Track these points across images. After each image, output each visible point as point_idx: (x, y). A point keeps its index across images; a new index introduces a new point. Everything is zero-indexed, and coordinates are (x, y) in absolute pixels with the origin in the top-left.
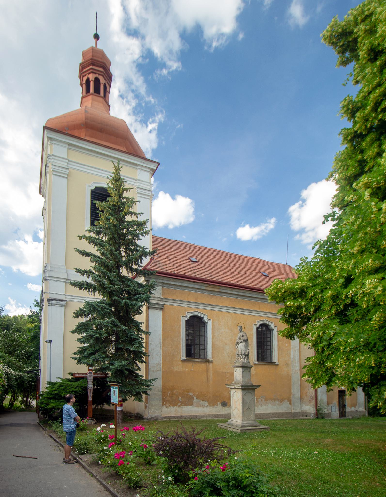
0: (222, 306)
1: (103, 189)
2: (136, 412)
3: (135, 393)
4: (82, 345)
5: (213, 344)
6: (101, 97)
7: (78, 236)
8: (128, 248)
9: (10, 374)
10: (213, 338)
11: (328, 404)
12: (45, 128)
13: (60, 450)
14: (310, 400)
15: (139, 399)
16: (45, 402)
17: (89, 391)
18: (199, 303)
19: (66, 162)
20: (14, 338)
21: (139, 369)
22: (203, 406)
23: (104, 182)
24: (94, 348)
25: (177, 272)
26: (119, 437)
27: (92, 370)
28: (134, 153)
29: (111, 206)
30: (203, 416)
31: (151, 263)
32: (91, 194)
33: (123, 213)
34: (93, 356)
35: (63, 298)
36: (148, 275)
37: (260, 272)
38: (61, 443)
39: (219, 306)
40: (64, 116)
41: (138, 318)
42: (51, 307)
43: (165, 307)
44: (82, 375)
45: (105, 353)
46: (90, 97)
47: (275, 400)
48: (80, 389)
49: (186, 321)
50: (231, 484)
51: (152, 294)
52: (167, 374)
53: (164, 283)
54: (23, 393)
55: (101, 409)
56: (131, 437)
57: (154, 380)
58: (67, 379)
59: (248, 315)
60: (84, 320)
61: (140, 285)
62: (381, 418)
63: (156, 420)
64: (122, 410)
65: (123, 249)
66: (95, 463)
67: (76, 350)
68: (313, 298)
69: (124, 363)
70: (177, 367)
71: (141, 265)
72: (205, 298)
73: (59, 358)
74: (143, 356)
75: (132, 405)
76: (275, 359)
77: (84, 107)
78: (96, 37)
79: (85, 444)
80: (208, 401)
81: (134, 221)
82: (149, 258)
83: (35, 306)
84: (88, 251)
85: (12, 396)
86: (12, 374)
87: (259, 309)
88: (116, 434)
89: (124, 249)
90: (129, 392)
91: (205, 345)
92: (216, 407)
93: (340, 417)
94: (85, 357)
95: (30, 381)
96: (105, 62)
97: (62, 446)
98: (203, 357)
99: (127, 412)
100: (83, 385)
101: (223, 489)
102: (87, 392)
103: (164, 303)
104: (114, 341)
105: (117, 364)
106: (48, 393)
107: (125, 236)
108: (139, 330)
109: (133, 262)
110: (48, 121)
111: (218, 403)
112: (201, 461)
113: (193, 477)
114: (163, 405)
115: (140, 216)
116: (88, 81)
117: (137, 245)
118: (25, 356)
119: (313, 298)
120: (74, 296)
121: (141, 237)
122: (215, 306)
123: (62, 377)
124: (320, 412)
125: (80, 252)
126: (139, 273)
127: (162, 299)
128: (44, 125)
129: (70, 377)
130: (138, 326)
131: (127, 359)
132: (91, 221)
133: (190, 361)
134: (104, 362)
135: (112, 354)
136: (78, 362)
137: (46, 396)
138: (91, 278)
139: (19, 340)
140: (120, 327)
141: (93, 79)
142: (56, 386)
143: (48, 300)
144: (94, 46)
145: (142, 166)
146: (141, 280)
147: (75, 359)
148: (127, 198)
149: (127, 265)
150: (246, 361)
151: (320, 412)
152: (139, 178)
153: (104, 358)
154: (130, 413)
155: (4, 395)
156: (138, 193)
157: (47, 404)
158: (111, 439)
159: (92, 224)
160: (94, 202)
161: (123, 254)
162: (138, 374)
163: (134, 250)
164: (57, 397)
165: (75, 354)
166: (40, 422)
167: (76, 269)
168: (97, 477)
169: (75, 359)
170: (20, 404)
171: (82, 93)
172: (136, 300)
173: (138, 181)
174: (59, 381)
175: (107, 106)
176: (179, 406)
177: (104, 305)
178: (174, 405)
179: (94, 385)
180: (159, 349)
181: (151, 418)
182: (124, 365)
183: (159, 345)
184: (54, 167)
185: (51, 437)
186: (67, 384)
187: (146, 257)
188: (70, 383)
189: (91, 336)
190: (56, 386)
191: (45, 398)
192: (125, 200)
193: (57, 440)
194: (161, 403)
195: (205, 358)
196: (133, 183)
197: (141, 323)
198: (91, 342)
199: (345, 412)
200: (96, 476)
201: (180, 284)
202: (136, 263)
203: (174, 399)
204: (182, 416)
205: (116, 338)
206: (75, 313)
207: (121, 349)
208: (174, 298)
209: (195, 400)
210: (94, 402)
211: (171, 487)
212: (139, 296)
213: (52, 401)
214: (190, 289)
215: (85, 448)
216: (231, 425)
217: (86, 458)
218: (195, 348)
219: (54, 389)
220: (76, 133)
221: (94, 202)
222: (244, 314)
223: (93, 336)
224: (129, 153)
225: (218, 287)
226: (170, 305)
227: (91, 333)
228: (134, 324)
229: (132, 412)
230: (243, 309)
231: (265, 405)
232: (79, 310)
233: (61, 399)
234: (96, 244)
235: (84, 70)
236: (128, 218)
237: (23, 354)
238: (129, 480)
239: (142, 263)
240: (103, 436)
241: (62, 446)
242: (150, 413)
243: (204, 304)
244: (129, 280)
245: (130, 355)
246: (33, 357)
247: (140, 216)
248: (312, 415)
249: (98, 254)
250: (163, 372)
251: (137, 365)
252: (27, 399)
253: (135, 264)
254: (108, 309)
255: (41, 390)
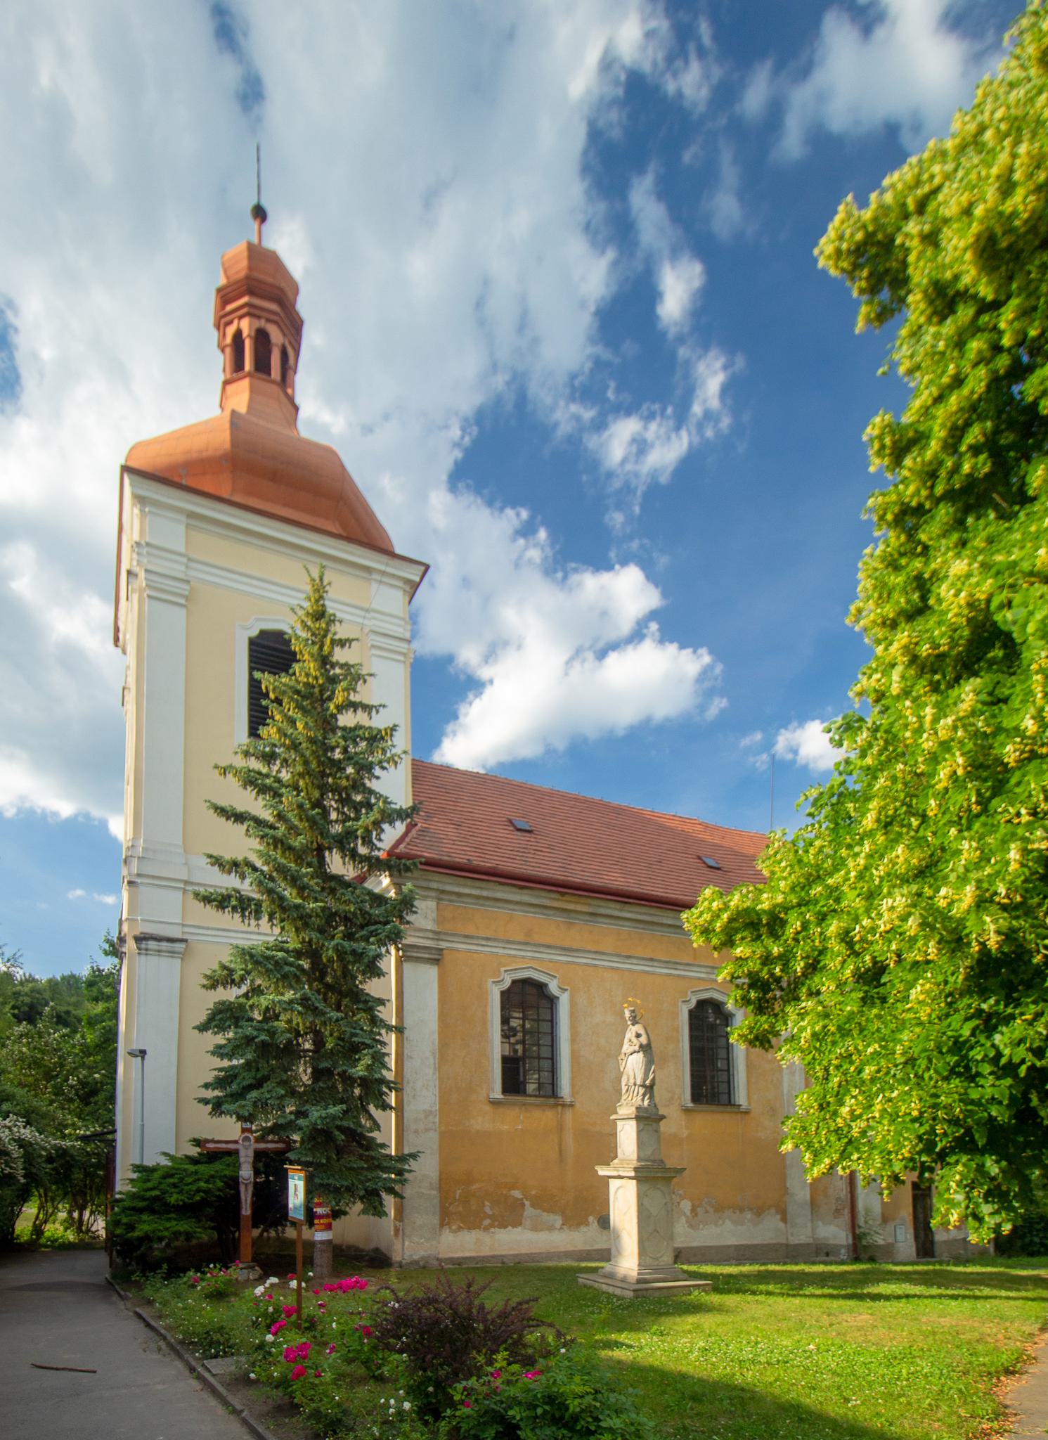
0: (596, 952)
1: (279, 636)
2: (373, 1246)
3: (362, 1193)
4: (226, 1063)
5: (574, 1056)
6: (273, 382)
7: (216, 767)
8: (345, 801)
9: (31, 1144)
10: (573, 1040)
11: (885, 1219)
12: (126, 469)
13: (160, 1350)
14: (837, 1211)
15: (375, 1208)
16: (125, 1220)
17: (242, 1188)
18: (535, 945)
19: (181, 563)
20: (46, 1044)
21: (376, 1126)
22: (551, 1228)
23: (286, 618)
24: (258, 1070)
25: (477, 862)
26: (310, 1309)
27: (250, 1130)
28: (363, 539)
29: (300, 687)
30: (550, 1256)
31: (410, 835)
32: (251, 650)
33: (332, 707)
34: (254, 1094)
35: (176, 933)
36: (399, 871)
37: (699, 858)
38: (163, 1331)
39: (589, 952)
40: (175, 436)
41: (372, 987)
42: (143, 957)
43: (448, 956)
44: (224, 1146)
45: (283, 1083)
46: (245, 383)
47: (742, 1210)
48: (220, 1184)
49: (502, 993)
50: (539, 1411)
51: (408, 923)
52: (452, 1139)
53: (443, 892)
54: (70, 1196)
55: (278, 1238)
56: (346, 1311)
57: (414, 1156)
58: (187, 1157)
59: (667, 975)
60: (231, 994)
61: (379, 899)
62: (1030, 1259)
63: (424, 1267)
64: (329, 1242)
65: (333, 803)
66: (242, 1381)
67: (210, 1077)
68: (800, 937)
69: (335, 1110)
70: (480, 1119)
71: (379, 845)
72: (550, 928)
73: (164, 1102)
74: (385, 1089)
75: (355, 1225)
76: (741, 1097)
77: (228, 413)
78: (260, 214)
79: (221, 1329)
80: (564, 1215)
81: (361, 727)
82: (400, 827)
83: (106, 953)
84: (240, 808)
85: (41, 1207)
86: (37, 1144)
87: (695, 959)
88: (299, 1302)
89: (336, 801)
90: (348, 1189)
91: (552, 1059)
92: (583, 1229)
93: (918, 1254)
94: (232, 1095)
95: (93, 1165)
96: (283, 285)
97: (165, 1338)
98: (550, 1093)
99: (349, 1247)
100: (227, 1173)
101: (522, 1424)
102: (238, 1193)
103: (444, 945)
104: (309, 1050)
105: (316, 1113)
106: (133, 1196)
107: (338, 766)
108: (374, 1021)
109: (357, 837)
110: (133, 448)
111: (591, 1219)
112: (481, 1359)
113: (462, 1402)
114: (442, 1225)
115: (377, 712)
116: (238, 335)
117: (371, 792)
118: (77, 1094)
119: (800, 937)
120: (208, 928)
121: (377, 771)
122: (577, 950)
123: (172, 1152)
124: (864, 1242)
125: (223, 812)
126: (376, 865)
127: (438, 935)
128: (123, 462)
129: (194, 1151)
130: (370, 1010)
131: (342, 1101)
132: (251, 722)
133: (514, 1104)
134: (282, 1108)
135: (305, 1086)
136: (213, 1109)
137: (127, 1204)
138: (248, 881)
139: (60, 1049)
140: (324, 1014)
141: (253, 334)
142: (156, 1175)
143: (138, 939)
144: (255, 241)
145: (383, 573)
146: (383, 883)
147: (205, 1101)
148: (342, 666)
149: (343, 843)
150: (646, 1103)
151: (864, 1242)
152: (375, 606)
153: (281, 1098)
154: (357, 1249)
155: (16, 1204)
156: (373, 646)
157: (131, 1227)
158: (289, 1316)
159: (253, 733)
160: (257, 675)
161: (334, 816)
162: (374, 1139)
163: (361, 804)
164: (157, 1206)
165: (206, 1086)
166: (114, 1277)
167: (211, 856)
168: (244, 1415)
169: (205, 1101)
170: (62, 1228)
171: (224, 370)
172: (366, 939)
173: (372, 614)
174: (164, 1162)
175: (290, 407)
176: (486, 1229)
177: (280, 954)
178: (472, 1226)
179: (257, 1173)
180: (431, 1071)
181: (411, 1263)
182: (334, 1117)
183: (432, 1061)
184: (152, 577)
185: (139, 1316)
186: (185, 1170)
187: (391, 823)
188: (192, 1168)
189: (249, 1040)
190: (156, 1175)
191: (124, 1210)
192: (338, 671)
193: (153, 1323)
194: (436, 1221)
195: (554, 1094)
196: (361, 620)
197: (381, 1002)
198: (249, 1056)
199: (932, 1242)
200: (242, 1411)
201: (485, 893)
202: (367, 841)
203: (473, 1208)
204: (493, 1257)
205: (315, 1043)
206: (206, 976)
207: (328, 1072)
208: (470, 930)
209: (529, 1211)
210: (257, 1219)
211: (406, 1427)
212: (373, 928)
213: (144, 1217)
214: (511, 906)
215: (222, 1340)
216: (611, 1276)
217: (222, 1367)
218: (527, 1068)
219: (149, 1185)
220: (207, 485)
221: (257, 675)
222: (653, 974)
223: (254, 1038)
224: (349, 539)
225: (583, 900)
226: (458, 950)
227: (249, 1031)
228: (361, 1006)
229: (362, 1246)
230: (652, 960)
231: (716, 1225)
232: (216, 967)
233: (168, 1212)
234: (262, 790)
235: (229, 308)
236: (347, 719)
237: (72, 1087)
238: (316, 1415)
239: (380, 840)
240: (271, 1309)
241: (165, 1338)
242: (408, 1249)
243: (549, 947)
244: (347, 885)
245: (352, 1087)
246: (96, 1096)
247: (377, 712)
248: (843, 1251)
249: (267, 815)
250: (442, 1134)
251: (371, 1117)
252: (81, 1215)
253: (363, 844)
254: (291, 965)
255: (118, 1188)
